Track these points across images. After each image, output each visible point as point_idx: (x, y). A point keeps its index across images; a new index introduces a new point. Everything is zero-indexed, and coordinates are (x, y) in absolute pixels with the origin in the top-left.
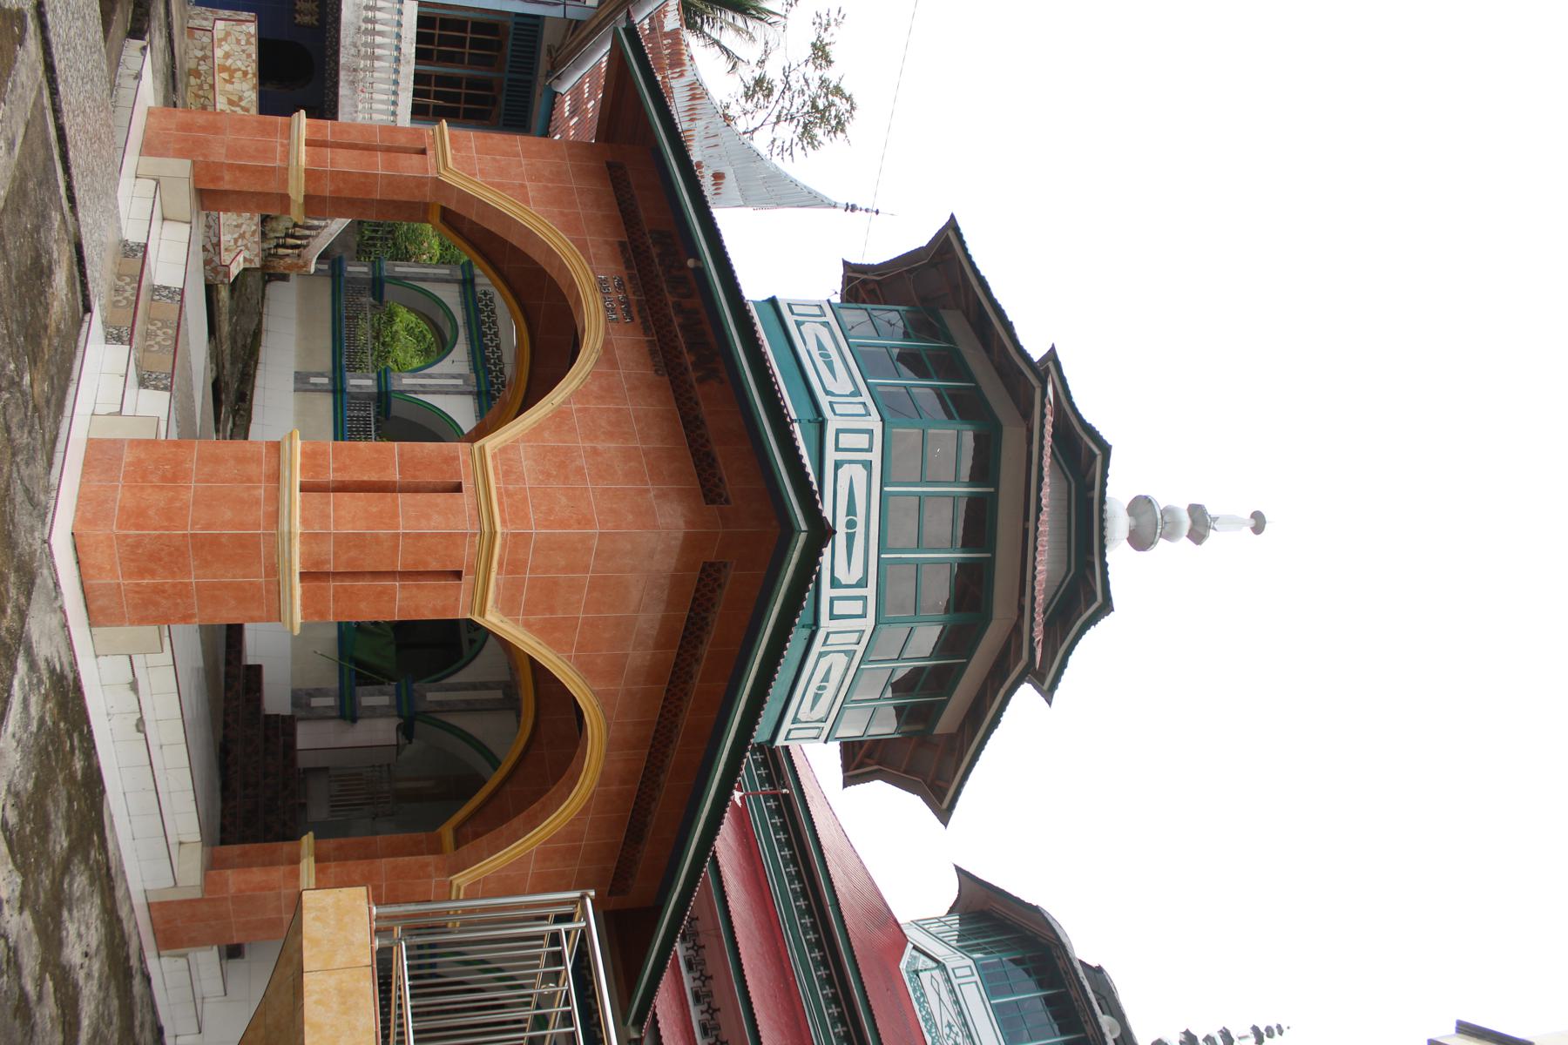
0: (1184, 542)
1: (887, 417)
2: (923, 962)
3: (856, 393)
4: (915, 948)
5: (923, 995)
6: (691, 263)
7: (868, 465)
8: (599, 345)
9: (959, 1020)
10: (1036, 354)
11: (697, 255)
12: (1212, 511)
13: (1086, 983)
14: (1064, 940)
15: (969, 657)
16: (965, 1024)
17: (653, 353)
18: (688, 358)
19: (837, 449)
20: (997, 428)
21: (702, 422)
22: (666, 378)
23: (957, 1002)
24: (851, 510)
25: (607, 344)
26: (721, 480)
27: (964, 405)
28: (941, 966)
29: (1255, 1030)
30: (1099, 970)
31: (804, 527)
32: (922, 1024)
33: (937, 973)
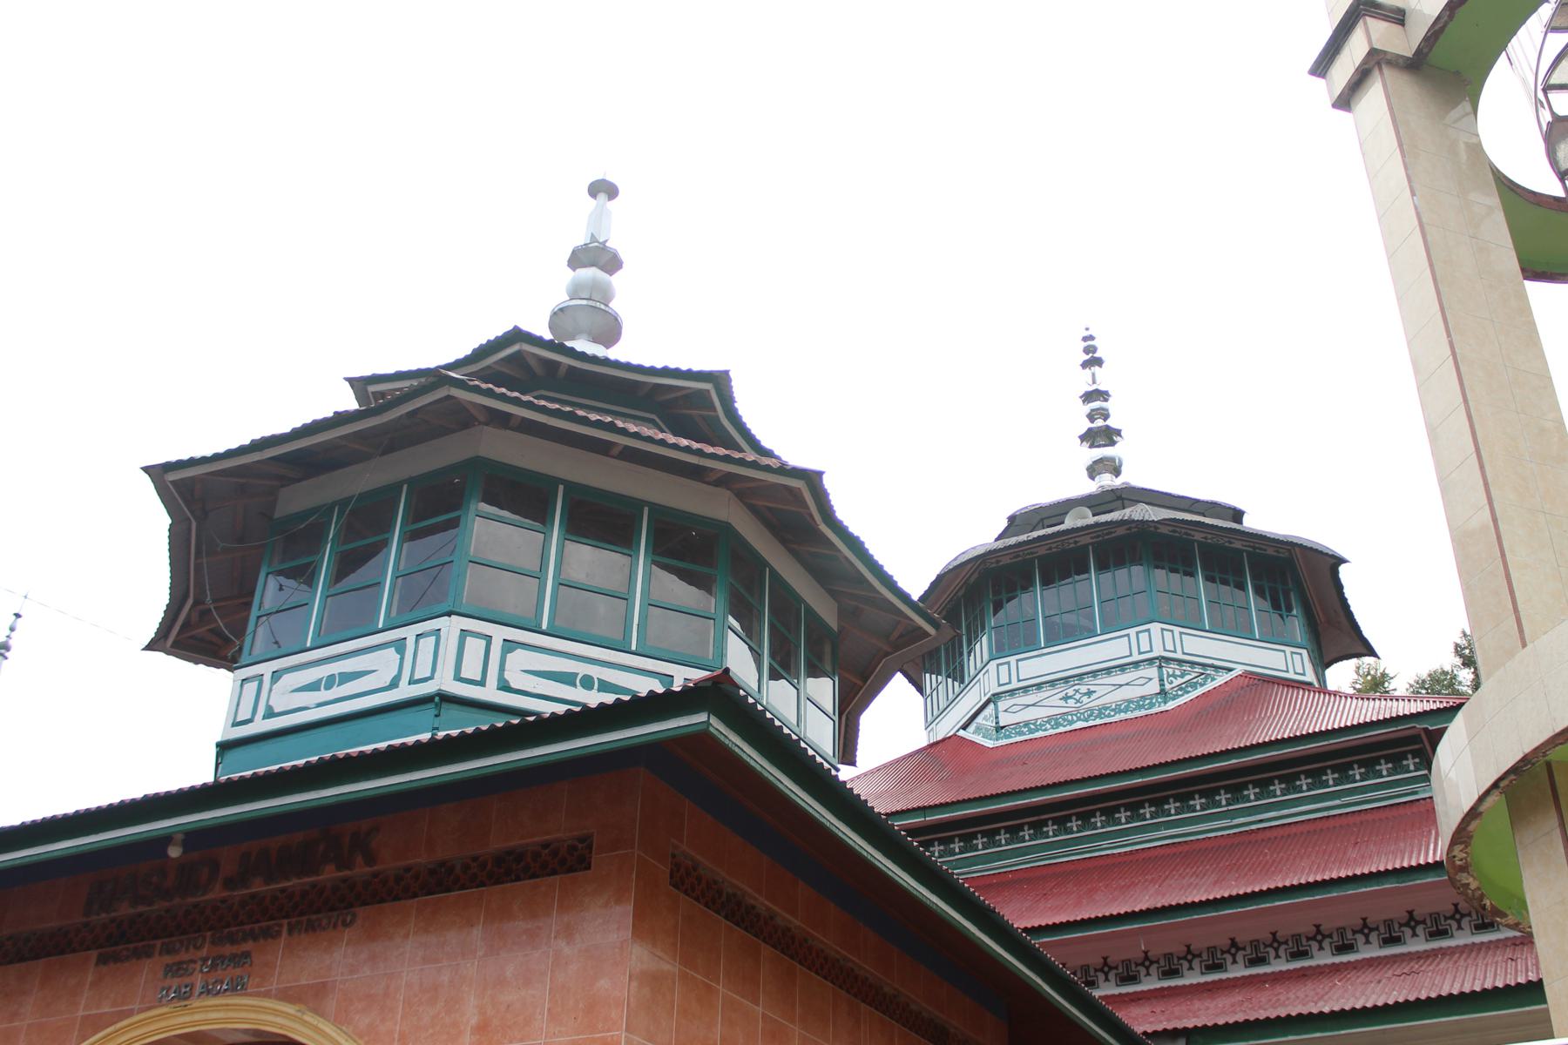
0: (617, 280)
1: (445, 608)
2: (986, 719)
3: (400, 645)
4: (964, 727)
5: (1027, 724)
6: (174, 852)
7: (510, 646)
8: (290, 1009)
9: (1061, 686)
10: (348, 402)
11: (164, 840)
12: (581, 239)
13: (1023, 538)
14: (981, 551)
15: (765, 564)
16: (1066, 679)
17: (312, 928)
18: (329, 874)
19: (482, 683)
20: (477, 464)
21: (443, 864)
22: (361, 912)
23: (1039, 686)
24: (567, 679)
25: (286, 996)
26: (546, 845)
27: (438, 505)
28: (994, 699)
29: (1085, 365)
30: (1012, 519)
31: (702, 717)
32: (1062, 729)
33: (1002, 705)
